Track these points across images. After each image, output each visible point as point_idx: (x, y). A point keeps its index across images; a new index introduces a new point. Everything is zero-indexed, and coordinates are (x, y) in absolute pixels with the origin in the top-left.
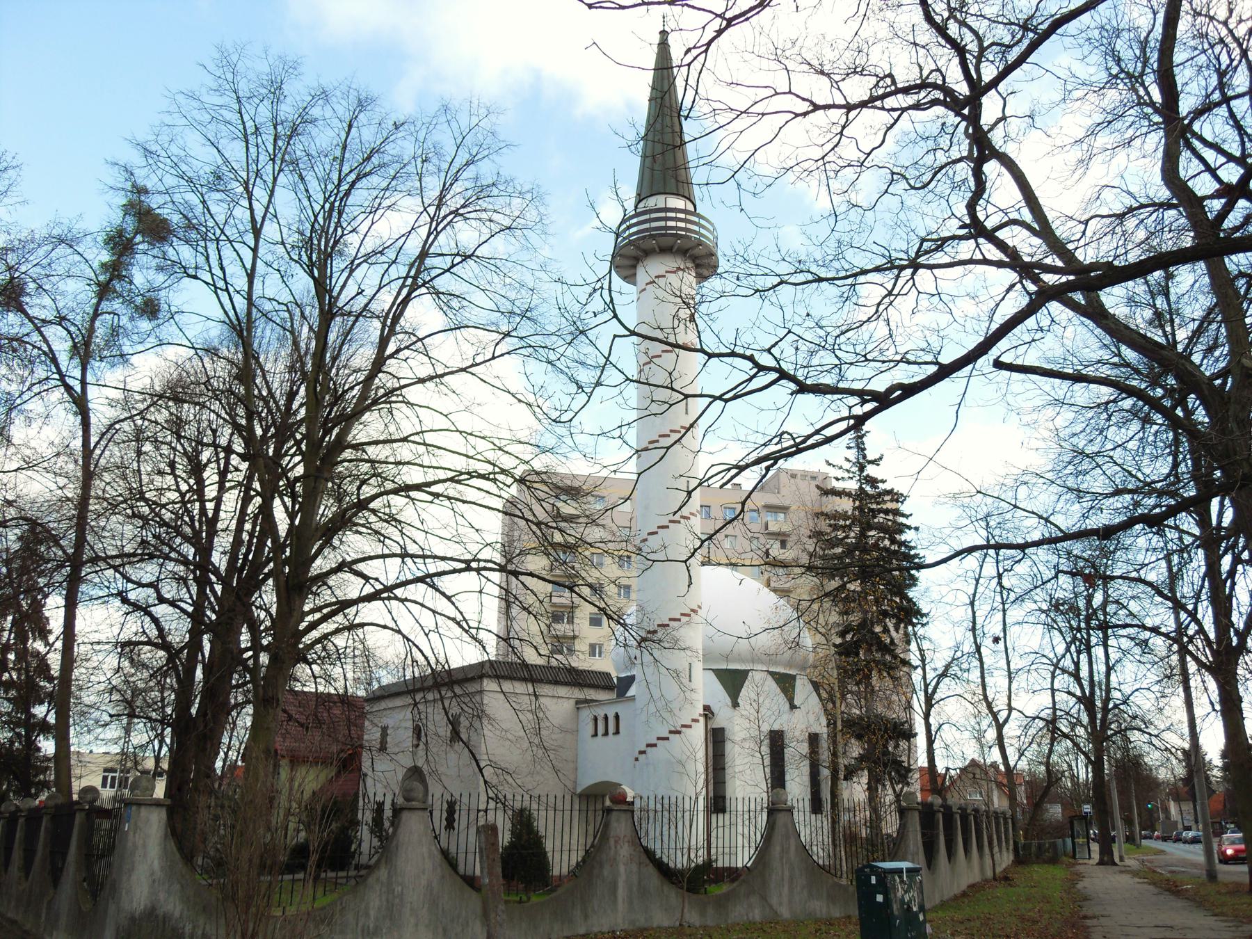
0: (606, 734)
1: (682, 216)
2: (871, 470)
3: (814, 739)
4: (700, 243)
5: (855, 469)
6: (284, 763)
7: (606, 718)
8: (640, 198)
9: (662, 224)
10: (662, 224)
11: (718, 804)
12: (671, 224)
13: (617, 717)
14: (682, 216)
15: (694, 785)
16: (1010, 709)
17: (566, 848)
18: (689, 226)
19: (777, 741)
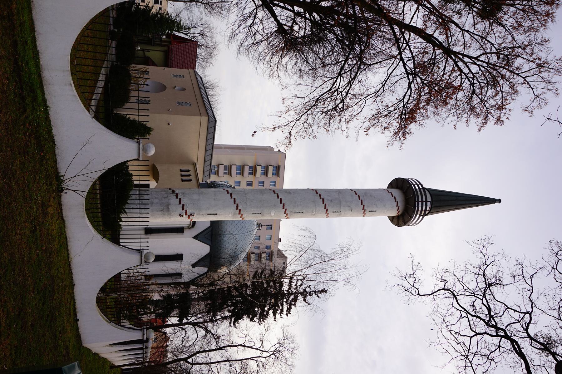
0: (182, 175)
1: (424, 210)
2: (300, 298)
3: (179, 275)
4: (411, 217)
5: (301, 290)
6: (165, 48)
7: (189, 175)
8: (429, 190)
9: (420, 200)
10: (420, 200)
11: (149, 231)
12: (420, 204)
13: (190, 180)
14: (424, 210)
15: (156, 221)
16: (193, 364)
17: (139, 240)
18: (419, 213)
19: (179, 257)
